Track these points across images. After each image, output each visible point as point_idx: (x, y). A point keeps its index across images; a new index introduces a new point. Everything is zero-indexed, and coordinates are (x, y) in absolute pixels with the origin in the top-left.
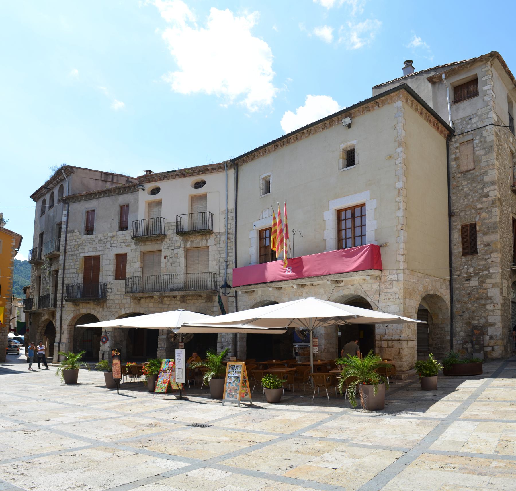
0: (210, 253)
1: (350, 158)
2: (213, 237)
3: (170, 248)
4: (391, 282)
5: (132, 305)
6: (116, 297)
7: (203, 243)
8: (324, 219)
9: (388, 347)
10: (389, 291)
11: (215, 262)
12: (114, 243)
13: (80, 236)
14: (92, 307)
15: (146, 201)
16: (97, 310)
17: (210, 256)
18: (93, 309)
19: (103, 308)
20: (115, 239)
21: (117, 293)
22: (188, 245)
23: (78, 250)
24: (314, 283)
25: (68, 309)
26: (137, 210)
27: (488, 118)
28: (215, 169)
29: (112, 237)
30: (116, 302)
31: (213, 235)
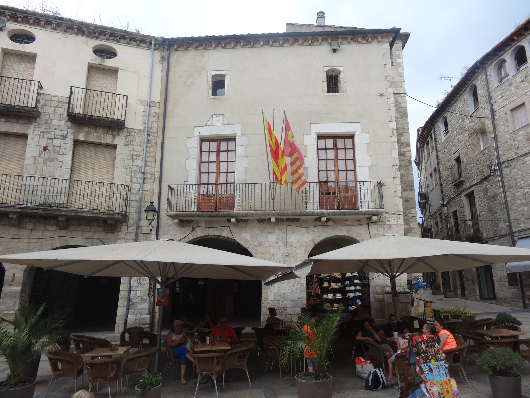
0: (117, 156)
1: (218, 84)
2: (124, 134)
3: (46, 136)
7: (108, 139)
8: (305, 143)
11: (124, 171)
17: (117, 160)
27: (401, 87)
28: (135, 41)
31: (125, 130)
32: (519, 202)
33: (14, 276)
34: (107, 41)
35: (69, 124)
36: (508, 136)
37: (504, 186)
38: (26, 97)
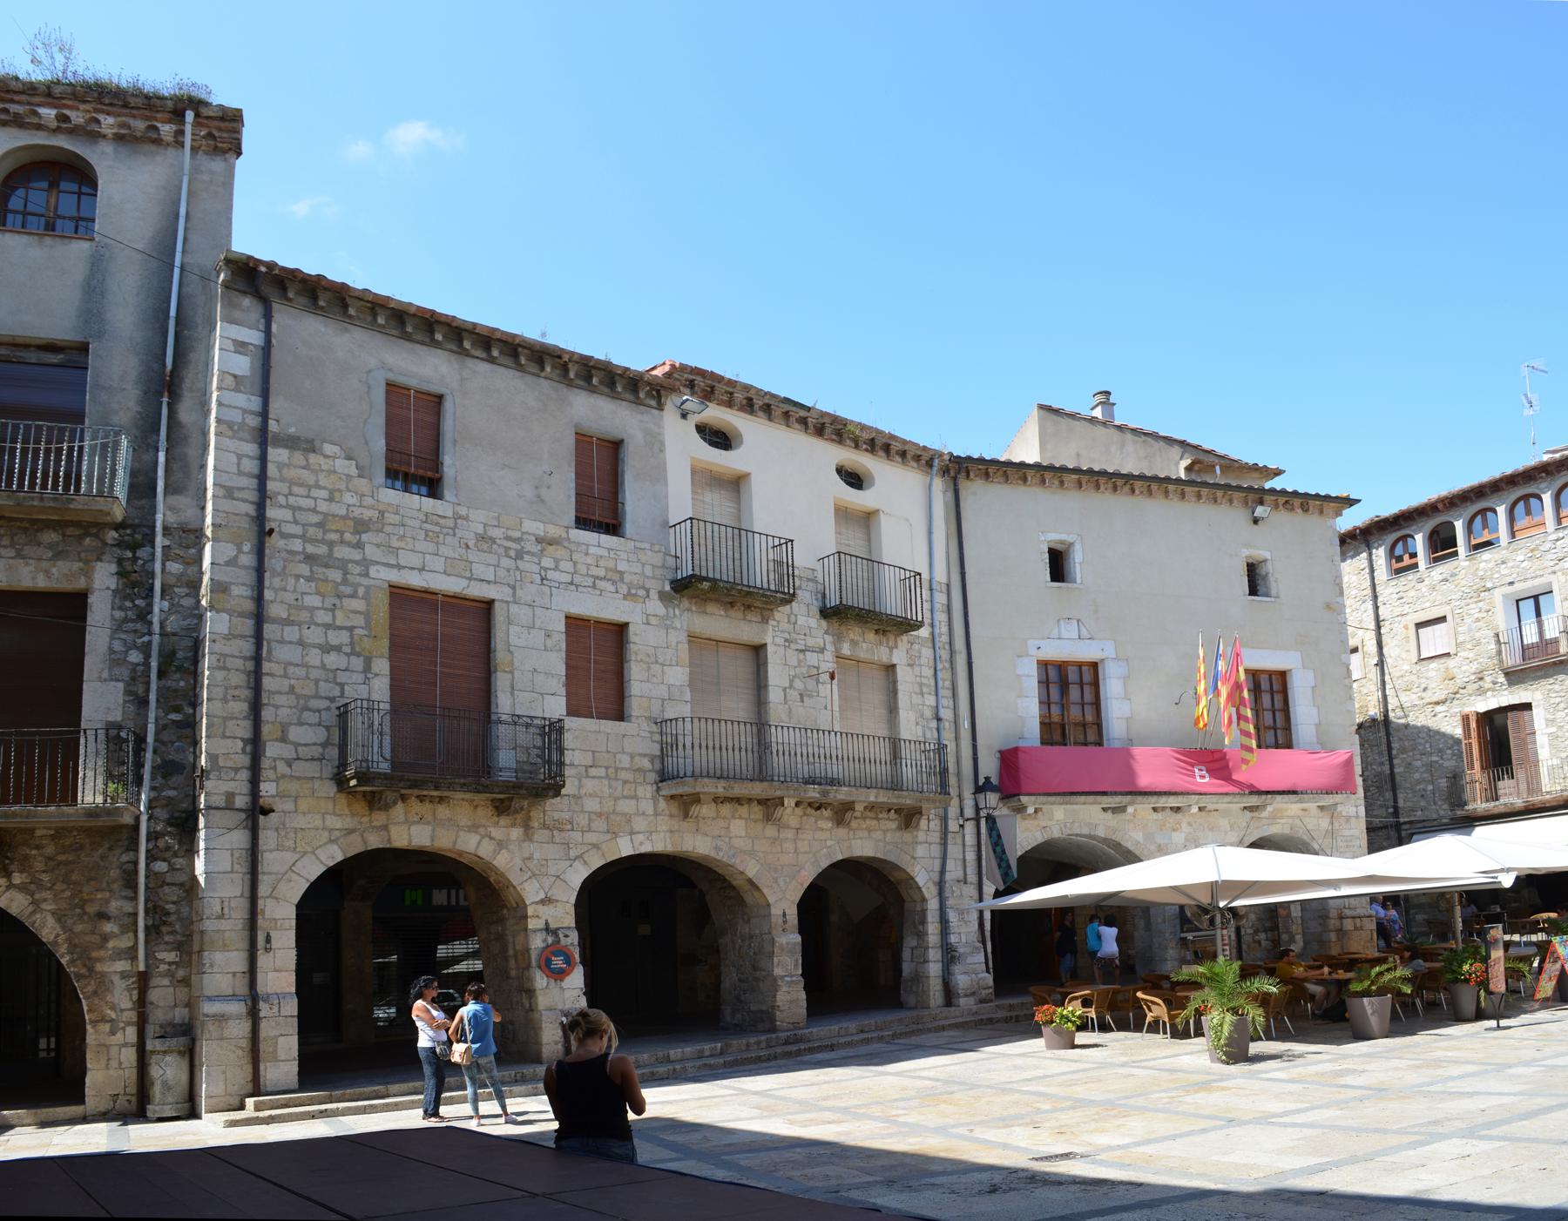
4: (1348, 819)
5: (664, 823)
6: (590, 785)
9: (1356, 928)
10: (1347, 833)
12: (556, 568)
13: (362, 484)
14: (464, 821)
15: (1071, 544)
16: (497, 833)
18: (473, 828)
19: (527, 826)
20: (561, 553)
21: (593, 772)
22: (846, 650)
23: (359, 546)
24: (1210, 807)
25: (300, 822)
26: (658, 475)
29: (545, 541)
30: (592, 805)
32: (1417, 776)
33: (784, 915)
34: (859, 445)
35: (824, 623)
36: (1406, 667)
37: (1390, 749)
38: (737, 563)
